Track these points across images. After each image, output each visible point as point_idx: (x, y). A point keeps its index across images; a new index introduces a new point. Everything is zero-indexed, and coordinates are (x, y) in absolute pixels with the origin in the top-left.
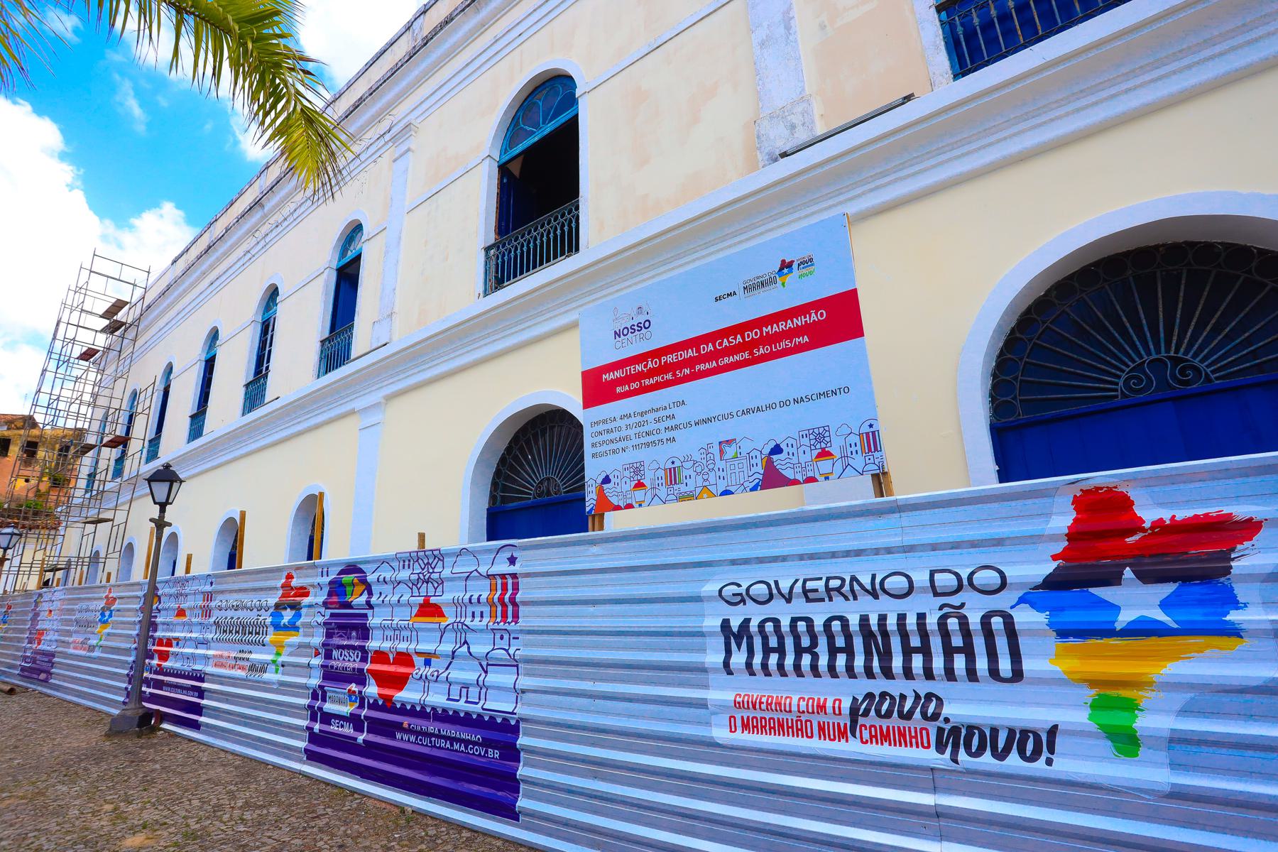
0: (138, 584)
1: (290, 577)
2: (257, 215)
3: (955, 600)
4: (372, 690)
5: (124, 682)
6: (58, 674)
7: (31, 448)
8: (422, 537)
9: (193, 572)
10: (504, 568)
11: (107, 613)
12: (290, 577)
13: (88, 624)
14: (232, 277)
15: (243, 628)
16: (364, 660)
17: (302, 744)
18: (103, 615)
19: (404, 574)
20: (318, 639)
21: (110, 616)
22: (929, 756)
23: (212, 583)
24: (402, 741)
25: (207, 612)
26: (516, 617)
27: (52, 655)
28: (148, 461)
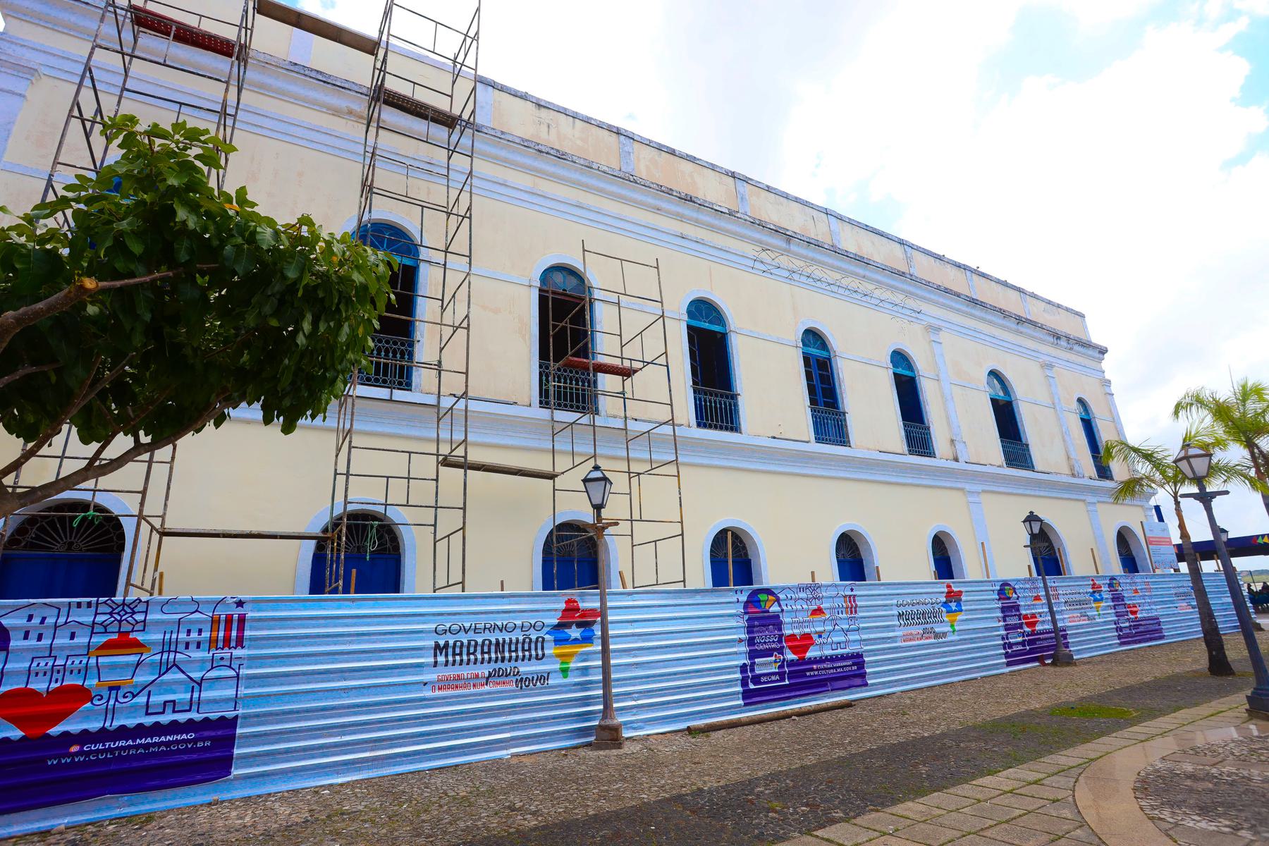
2: (778, 242)
3: (527, 633)
4: (1027, 629)
6: (1073, 643)
10: (850, 593)
14: (710, 258)
15: (1080, 602)
16: (1020, 619)
19: (802, 595)
22: (933, 641)
26: (856, 612)
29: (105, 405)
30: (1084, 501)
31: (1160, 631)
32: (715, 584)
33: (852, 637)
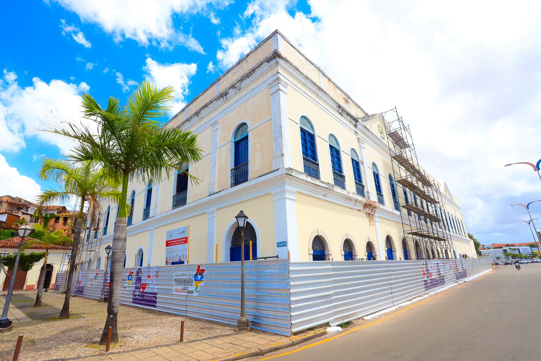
0: (103, 270)
1: (131, 270)
5: (132, 296)
7: (66, 219)
8: (149, 264)
9: (218, 262)
11: (96, 277)
12: (131, 270)
13: (92, 279)
17: (132, 301)
18: (95, 277)
20: (135, 282)
21: (97, 277)
23: (158, 269)
24: (145, 298)
25: (157, 276)
27: (59, 285)
28: (104, 235)
29: (12, 290)
30: (206, 213)
31: (155, 302)
32: (241, 261)
33: (156, 287)
